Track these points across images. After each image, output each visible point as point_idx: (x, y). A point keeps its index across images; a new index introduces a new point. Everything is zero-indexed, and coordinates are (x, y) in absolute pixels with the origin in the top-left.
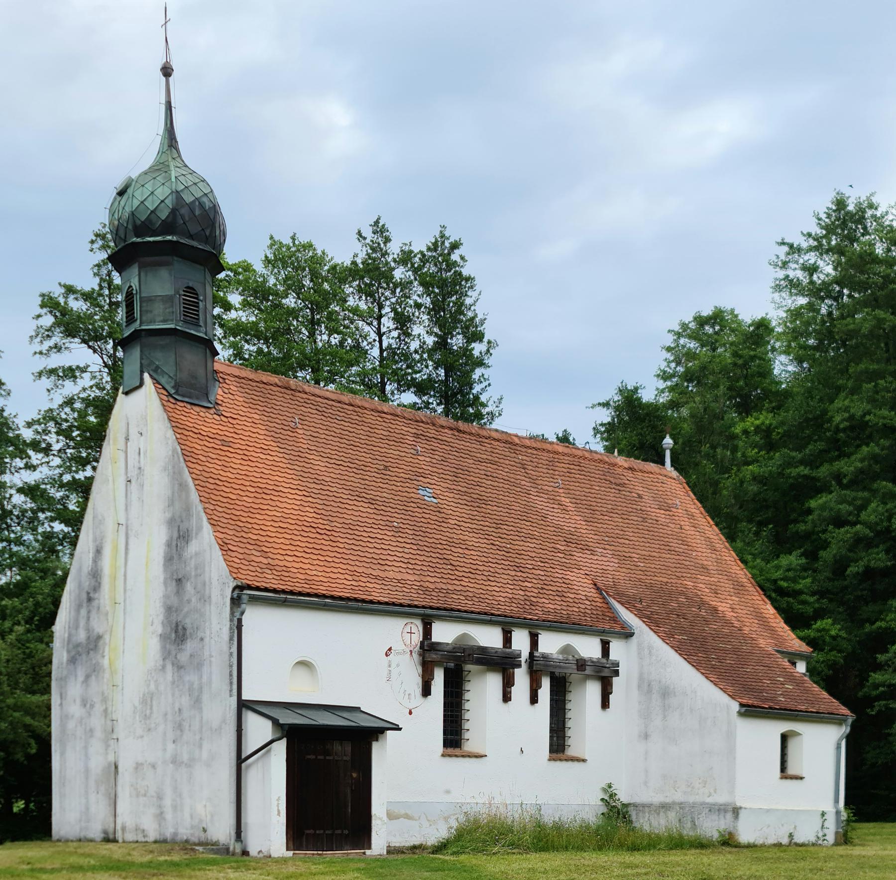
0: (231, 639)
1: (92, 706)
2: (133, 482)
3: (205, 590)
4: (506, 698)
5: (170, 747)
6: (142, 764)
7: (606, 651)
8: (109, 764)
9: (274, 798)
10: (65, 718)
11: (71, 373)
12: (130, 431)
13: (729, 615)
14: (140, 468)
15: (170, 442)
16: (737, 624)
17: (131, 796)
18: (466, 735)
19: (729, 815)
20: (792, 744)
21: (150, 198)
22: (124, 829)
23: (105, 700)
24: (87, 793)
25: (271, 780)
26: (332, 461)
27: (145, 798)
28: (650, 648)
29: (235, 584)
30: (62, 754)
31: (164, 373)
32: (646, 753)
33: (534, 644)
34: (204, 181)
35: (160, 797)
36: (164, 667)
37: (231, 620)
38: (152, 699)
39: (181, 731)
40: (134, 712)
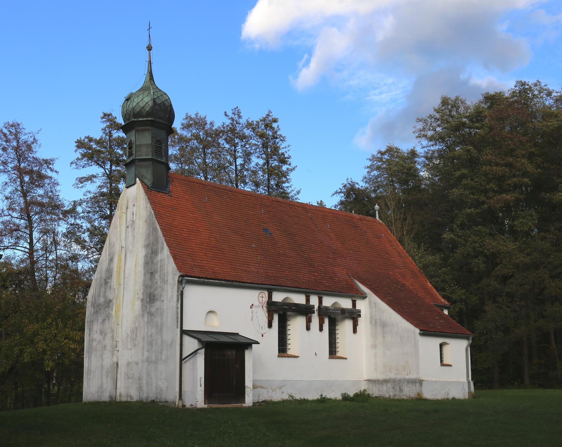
0: (178, 301)
1: (106, 335)
2: (130, 227)
4: (308, 328)
5: (146, 354)
6: (131, 363)
7: (354, 305)
8: (114, 363)
9: (199, 378)
10: (91, 341)
11: (90, 178)
13: (411, 287)
15: (148, 209)
16: (415, 292)
18: (289, 347)
19: (418, 385)
20: (445, 348)
22: (120, 395)
23: (113, 331)
24: (102, 377)
25: (198, 368)
28: (375, 304)
30: (89, 358)
31: (146, 178)
32: (375, 355)
33: (320, 302)
34: (166, 94)
35: (140, 379)
36: (143, 315)
37: (178, 292)
38: (136, 330)
39: (152, 346)
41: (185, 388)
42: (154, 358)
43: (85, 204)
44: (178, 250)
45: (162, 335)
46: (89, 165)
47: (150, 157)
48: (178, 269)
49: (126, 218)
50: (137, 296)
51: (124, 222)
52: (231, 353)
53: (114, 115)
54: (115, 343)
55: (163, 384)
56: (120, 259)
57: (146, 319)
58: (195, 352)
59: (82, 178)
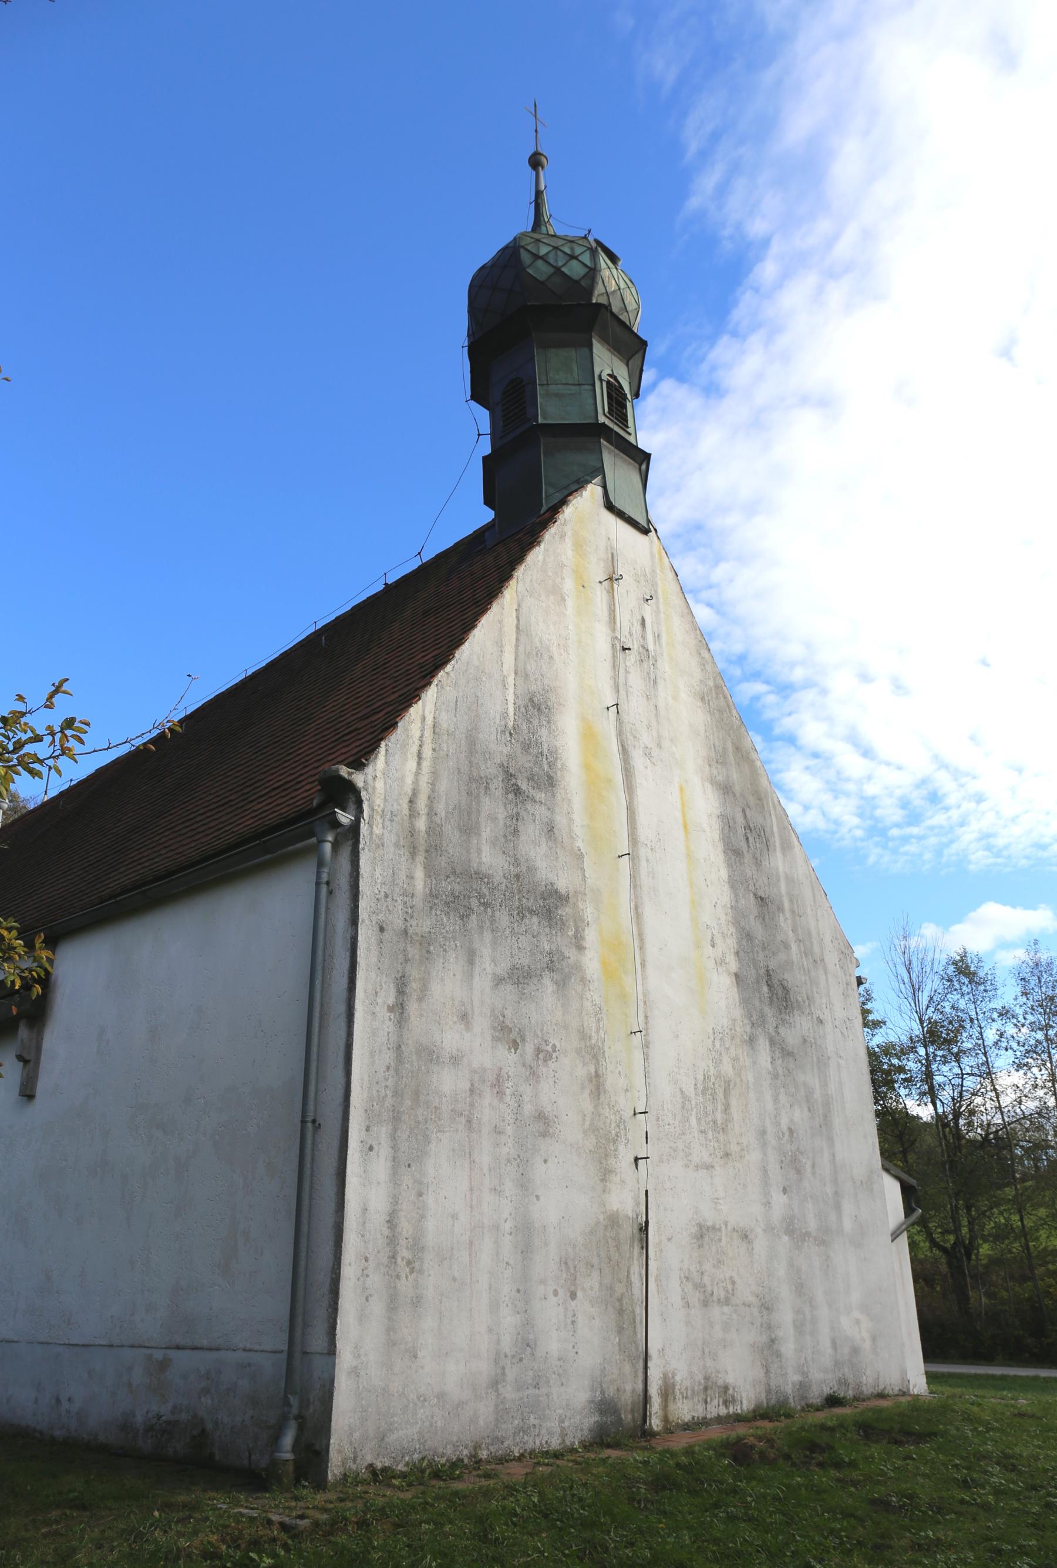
5: (779, 1200)
22: (667, 1392)
30: (405, 1163)
35: (767, 1307)
36: (751, 1040)
38: (727, 1092)
42: (812, 1225)
45: (830, 1140)
55: (855, 1328)
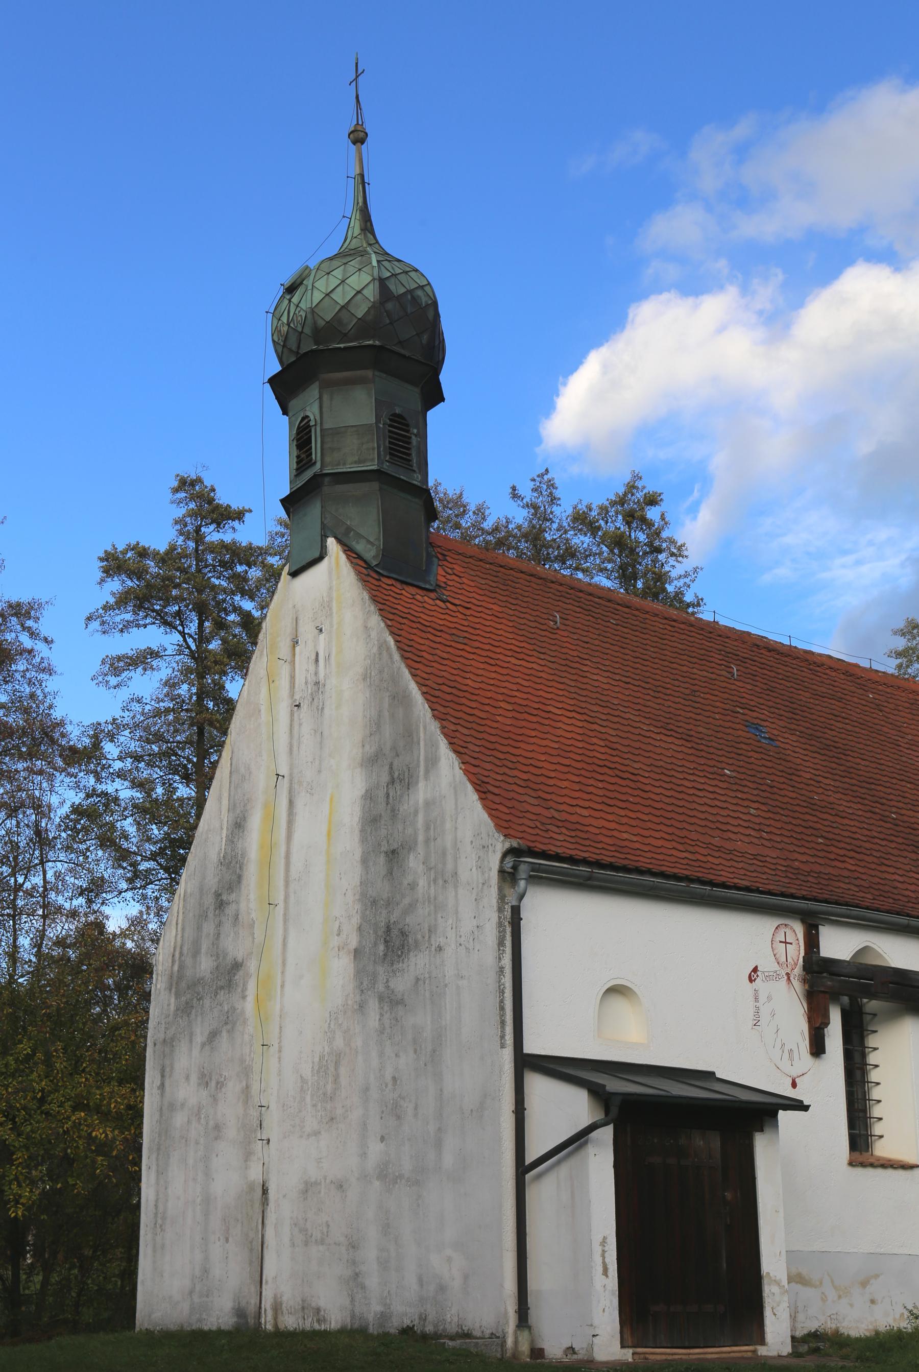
0: (501, 943)
1: (220, 1085)
2: (304, 707)
3: (444, 864)
5: (375, 1149)
6: (317, 1183)
8: (251, 1187)
9: (597, 1238)
10: (168, 1109)
11: (143, 659)
12: (301, 629)
14: (317, 683)
15: (374, 634)
17: (293, 1245)
21: (340, 288)
22: (277, 1308)
23: (246, 1072)
25: (588, 1201)
26: (617, 677)
27: (321, 1248)
29: (507, 845)
31: (359, 536)
34: (416, 270)
35: (353, 1246)
36: (361, 1007)
37: (500, 910)
38: (337, 1064)
40: (302, 1089)
41: (541, 1279)
43: (127, 733)
44: (488, 766)
46: (138, 626)
47: (374, 467)
48: (498, 827)
49: (292, 678)
50: (336, 941)
51: (284, 691)
52: (706, 1145)
53: (208, 482)
54: (254, 1113)
56: (270, 819)
57: (373, 1020)
58: (579, 1139)
59: (119, 658)
